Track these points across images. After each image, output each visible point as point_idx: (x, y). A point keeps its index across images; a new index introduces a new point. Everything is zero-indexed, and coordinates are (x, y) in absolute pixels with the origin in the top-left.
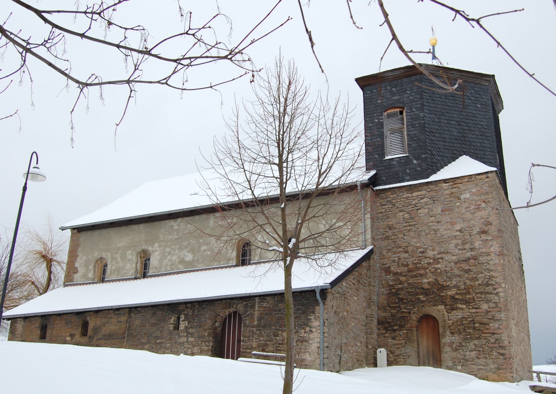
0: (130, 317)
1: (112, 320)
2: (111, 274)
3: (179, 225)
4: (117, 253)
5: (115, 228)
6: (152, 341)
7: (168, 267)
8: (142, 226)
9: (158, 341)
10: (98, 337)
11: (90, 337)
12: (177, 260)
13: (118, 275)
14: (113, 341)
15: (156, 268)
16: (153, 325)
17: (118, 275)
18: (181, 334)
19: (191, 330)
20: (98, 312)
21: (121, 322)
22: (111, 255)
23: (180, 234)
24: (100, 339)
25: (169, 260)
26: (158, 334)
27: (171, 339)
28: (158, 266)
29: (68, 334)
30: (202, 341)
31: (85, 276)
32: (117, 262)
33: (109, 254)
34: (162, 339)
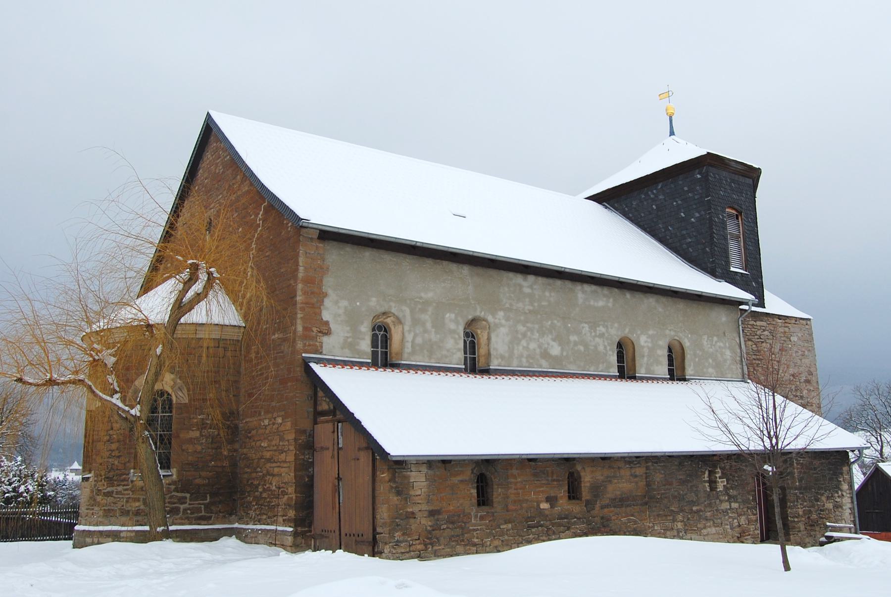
0: (647, 468)
1: (622, 472)
2: (413, 352)
3: (531, 287)
4: (423, 311)
5: (411, 257)
6: (687, 508)
7: (524, 360)
8: (466, 270)
9: (694, 508)
10: (603, 503)
11: (588, 503)
12: (538, 351)
13: (430, 358)
14: (629, 509)
15: (502, 357)
16: (683, 482)
17: (430, 358)
18: (722, 498)
19: (732, 492)
20: (605, 460)
21: (636, 476)
22: (412, 311)
23: (536, 304)
24: (607, 506)
25: (524, 347)
26: (692, 496)
27: (710, 505)
28: (507, 355)
29: (542, 497)
30: (748, 508)
31: (350, 345)
32: (425, 331)
33: (408, 311)
34: (698, 505)
